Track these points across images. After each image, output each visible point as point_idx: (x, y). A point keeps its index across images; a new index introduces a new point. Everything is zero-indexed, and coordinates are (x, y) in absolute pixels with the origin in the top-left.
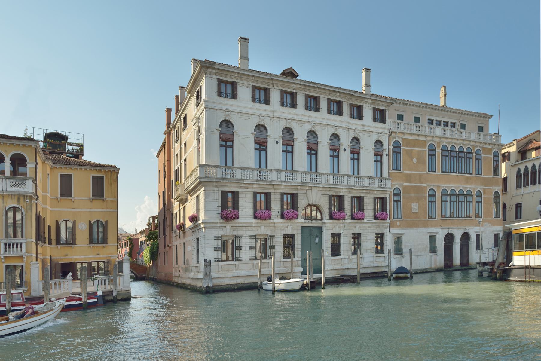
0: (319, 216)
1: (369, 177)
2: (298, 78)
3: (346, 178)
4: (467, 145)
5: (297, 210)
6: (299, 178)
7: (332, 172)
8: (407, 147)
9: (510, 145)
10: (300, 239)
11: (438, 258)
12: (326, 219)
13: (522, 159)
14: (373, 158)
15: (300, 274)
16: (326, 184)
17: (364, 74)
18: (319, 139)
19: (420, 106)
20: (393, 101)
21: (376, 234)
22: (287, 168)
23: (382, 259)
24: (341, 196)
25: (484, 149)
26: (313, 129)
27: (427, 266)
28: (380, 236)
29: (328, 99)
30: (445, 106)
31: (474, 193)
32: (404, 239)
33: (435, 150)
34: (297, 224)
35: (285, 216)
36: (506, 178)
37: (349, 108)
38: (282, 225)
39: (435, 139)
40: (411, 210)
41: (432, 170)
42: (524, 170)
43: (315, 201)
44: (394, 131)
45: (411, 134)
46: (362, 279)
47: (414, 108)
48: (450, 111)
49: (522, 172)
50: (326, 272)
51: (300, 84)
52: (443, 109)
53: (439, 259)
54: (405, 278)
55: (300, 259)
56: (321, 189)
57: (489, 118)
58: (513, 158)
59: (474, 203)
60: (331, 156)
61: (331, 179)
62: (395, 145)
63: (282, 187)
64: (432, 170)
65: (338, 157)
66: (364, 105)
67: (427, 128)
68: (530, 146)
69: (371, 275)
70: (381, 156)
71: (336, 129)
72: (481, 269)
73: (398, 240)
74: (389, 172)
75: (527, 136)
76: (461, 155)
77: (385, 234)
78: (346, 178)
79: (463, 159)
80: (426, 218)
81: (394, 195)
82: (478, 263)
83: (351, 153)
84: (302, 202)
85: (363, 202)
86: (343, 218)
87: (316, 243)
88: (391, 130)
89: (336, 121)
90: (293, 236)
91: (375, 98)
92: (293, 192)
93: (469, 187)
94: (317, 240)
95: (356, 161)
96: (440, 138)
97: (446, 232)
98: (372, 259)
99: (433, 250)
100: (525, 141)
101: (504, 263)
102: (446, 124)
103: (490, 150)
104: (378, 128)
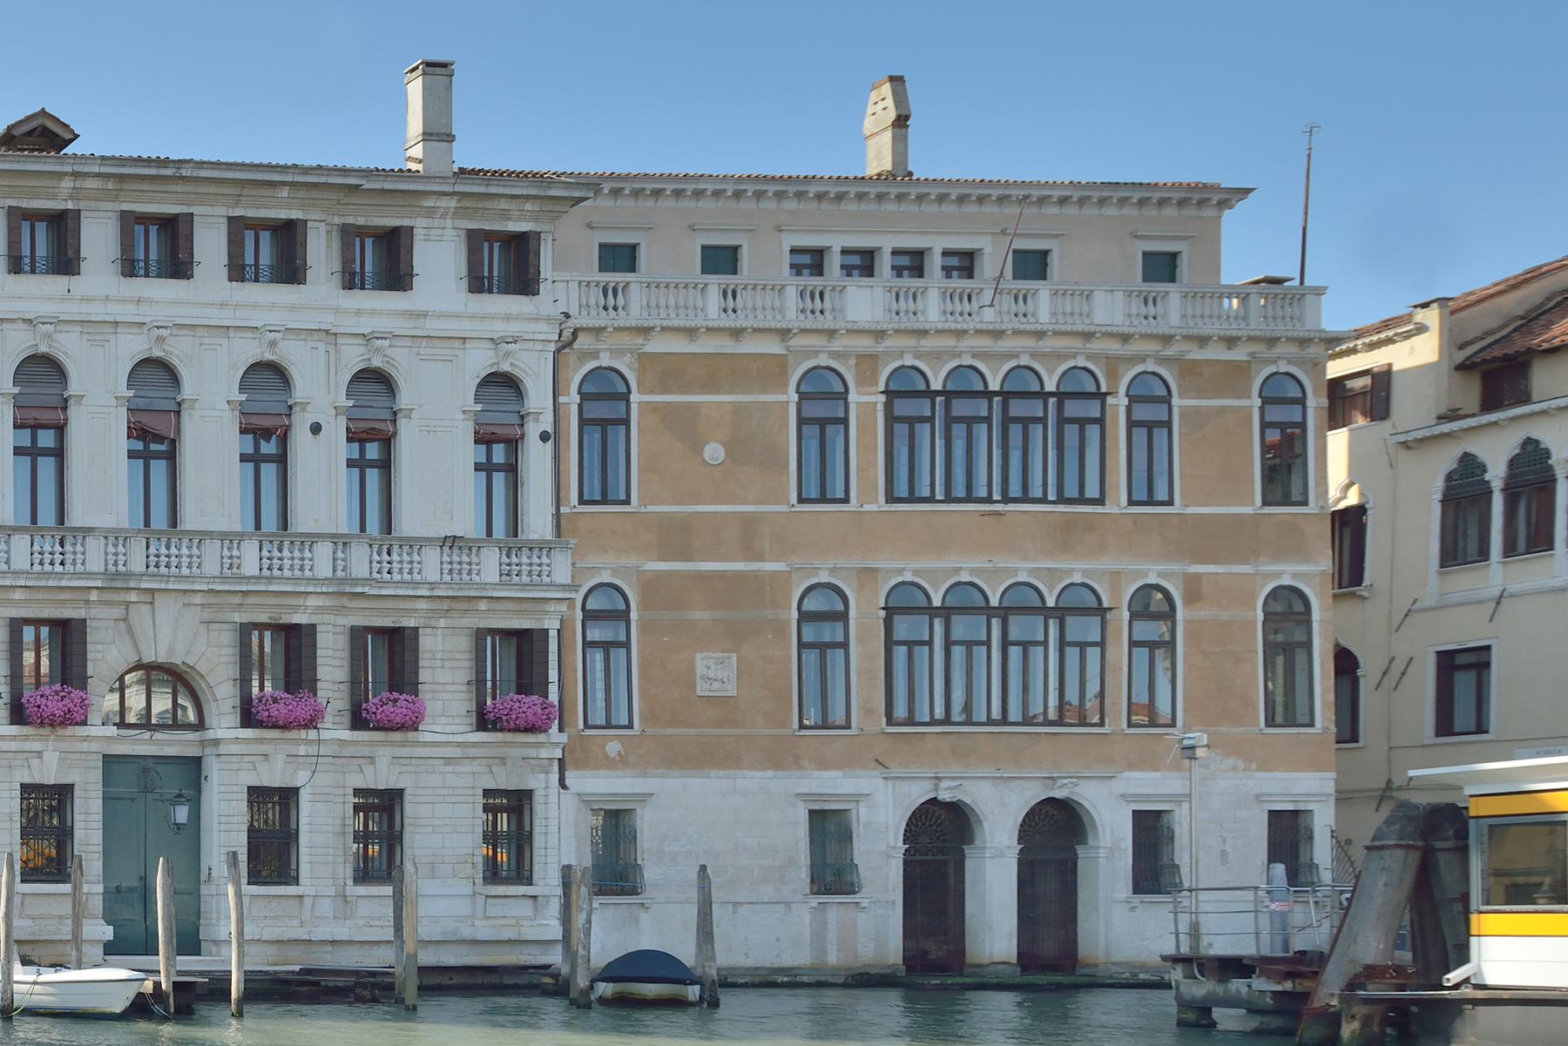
0: (192, 716)
1: (224, 537)
2: (69, 150)
3: (324, 551)
4: (1060, 356)
5: (84, 688)
6: (95, 556)
7: (251, 527)
8: (666, 390)
9: (1390, 329)
10: (96, 805)
11: (865, 923)
12: (224, 724)
13: (1490, 403)
14: (470, 453)
15: (100, 951)
16: (223, 578)
17: (415, 89)
18: (188, 390)
19: (738, 195)
20: (566, 193)
21: (487, 793)
22: (34, 520)
23: (526, 909)
24: (296, 628)
25: (1188, 369)
26: (157, 353)
27: (797, 956)
28: (510, 811)
29: (231, 220)
30: (900, 174)
31: (1120, 600)
32: (647, 824)
33: (843, 396)
34: (85, 746)
35: (30, 710)
36: (1359, 511)
37: (336, 245)
38: (13, 746)
39: (1097, 346)
40: (692, 686)
41: (822, 488)
42: (1513, 463)
43: (171, 651)
44: (591, 323)
45: (691, 332)
46: (424, 990)
47: (706, 204)
48: (942, 198)
49: (1496, 474)
50: (251, 950)
51: (99, 175)
52: (894, 191)
53: (876, 924)
54: (677, 1003)
55: (100, 888)
56: (198, 599)
57: (1224, 204)
58: (1411, 411)
59: (1119, 651)
60: (244, 458)
61: (250, 558)
62: (587, 389)
63: (18, 595)
64: (822, 488)
65: (282, 459)
66: (420, 224)
67: (791, 293)
68: (1556, 330)
69: (457, 979)
70: (514, 444)
71: (273, 344)
72: (1200, 988)
73: (615, 826)
74: (557, 515)
75: (1534, 275)
76: (1018, 408)
77: (538, 798)
78: (324, 551)
79: (981, 431)
80: (784, 724)
81: (590, 616)
82: (1177, 960)
83: (349, 440)
84: (106, 655)
85: (416, 650)
86: (311, 723)
87: (179, 826)
88: (572, 323)
89: (273, 307)
90: (63, 793)
91: (477, 184)
92: (67, 613)
93: (1077, 569)
94: (182, 814)
95: (47, 466)
96: (880, 334)
97: (918, 794)
98: (464, 907)
99: (832, 874)
100: (1516, 303)
101: (1399, 970)
102: (913, 263)
103: (1240, 371)
104: (493, 317)
